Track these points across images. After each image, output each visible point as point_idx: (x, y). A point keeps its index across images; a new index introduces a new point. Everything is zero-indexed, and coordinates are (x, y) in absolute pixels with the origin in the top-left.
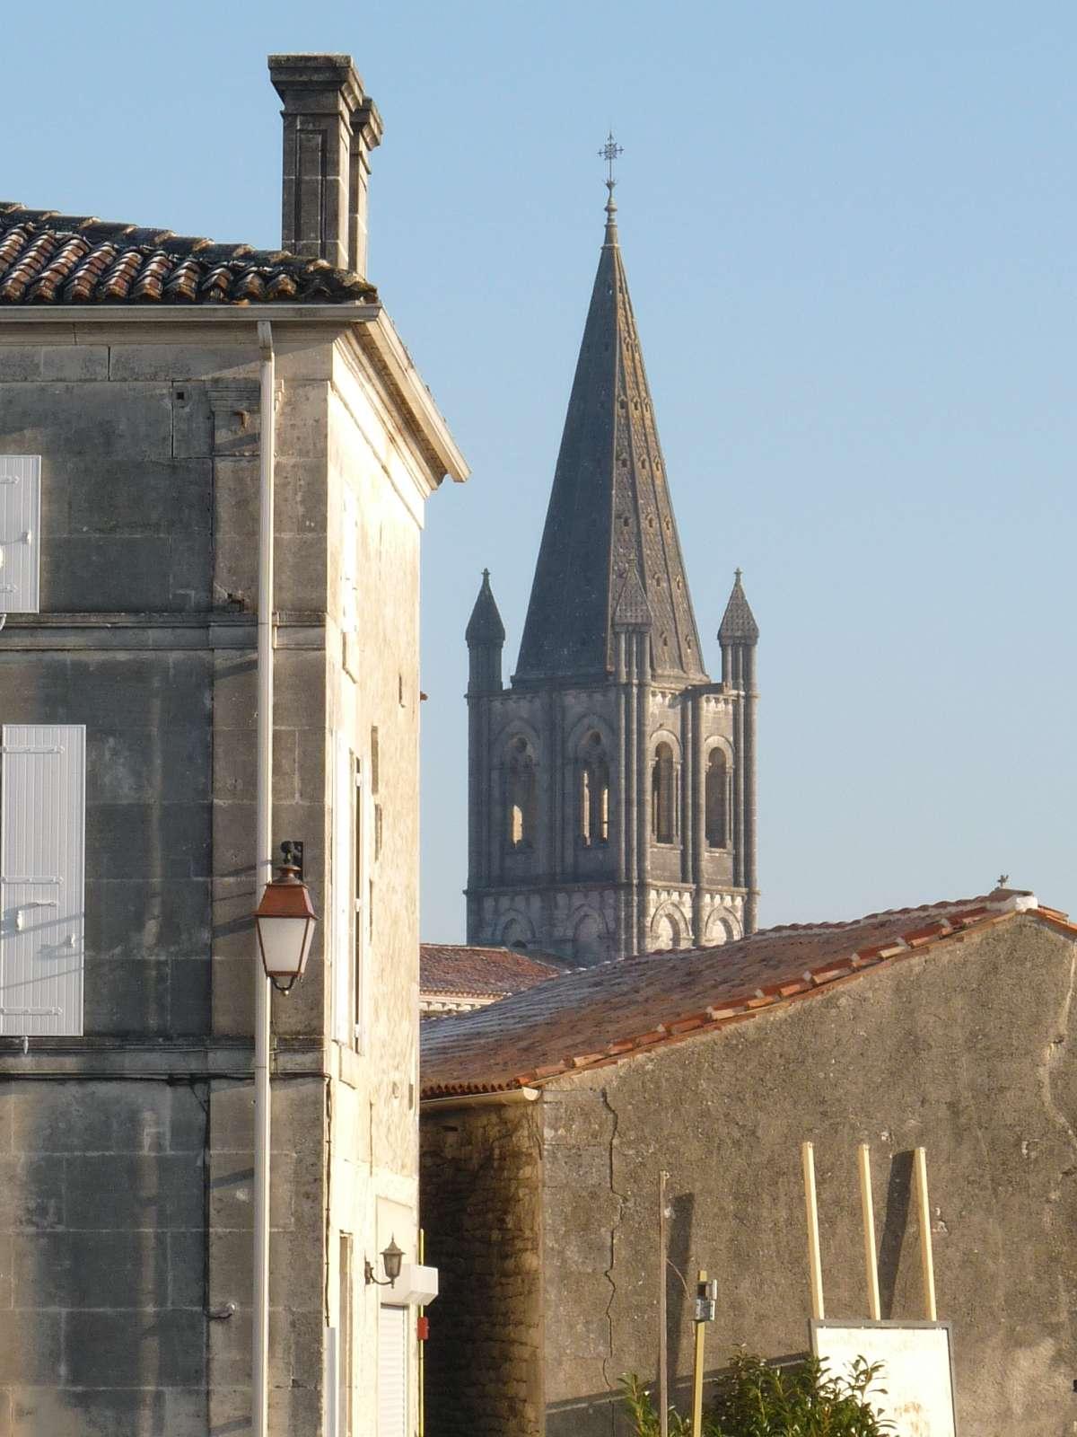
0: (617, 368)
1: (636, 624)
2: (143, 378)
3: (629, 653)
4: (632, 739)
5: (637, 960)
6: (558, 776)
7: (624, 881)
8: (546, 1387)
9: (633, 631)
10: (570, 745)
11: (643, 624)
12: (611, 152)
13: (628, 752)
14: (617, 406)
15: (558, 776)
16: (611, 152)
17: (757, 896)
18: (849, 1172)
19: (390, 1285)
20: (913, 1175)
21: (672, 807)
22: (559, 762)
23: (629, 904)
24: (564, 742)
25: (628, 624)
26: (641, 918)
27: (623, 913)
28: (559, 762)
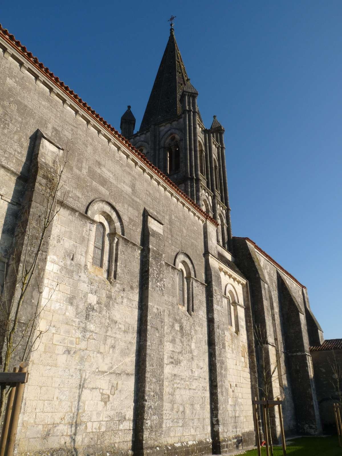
0: (176, 55)
1: (192, 93)
2: (23, 279)
3: (189, 102)
4: (191, 128)
5: (75, 415)
6: (157, 152)
7: (189, 176)
8: (219, 405)
9: (191, 95)
10: (162, 142)
11: (194, 93)
12: (172, 19)
13: (190, 133)
14: (177, 62)
15: (157, 152)
16: (172, 19)
17: (230, 211)
18: (222, 361)
19: (83, 210)
20: (315, 322)
21: (203, 166)
22: (157, 147)
23: (192, 187)
24: (159, 141)
25: (189, 92)
26: (197, 193)
27: (190, 190)
28: (157, 147)
